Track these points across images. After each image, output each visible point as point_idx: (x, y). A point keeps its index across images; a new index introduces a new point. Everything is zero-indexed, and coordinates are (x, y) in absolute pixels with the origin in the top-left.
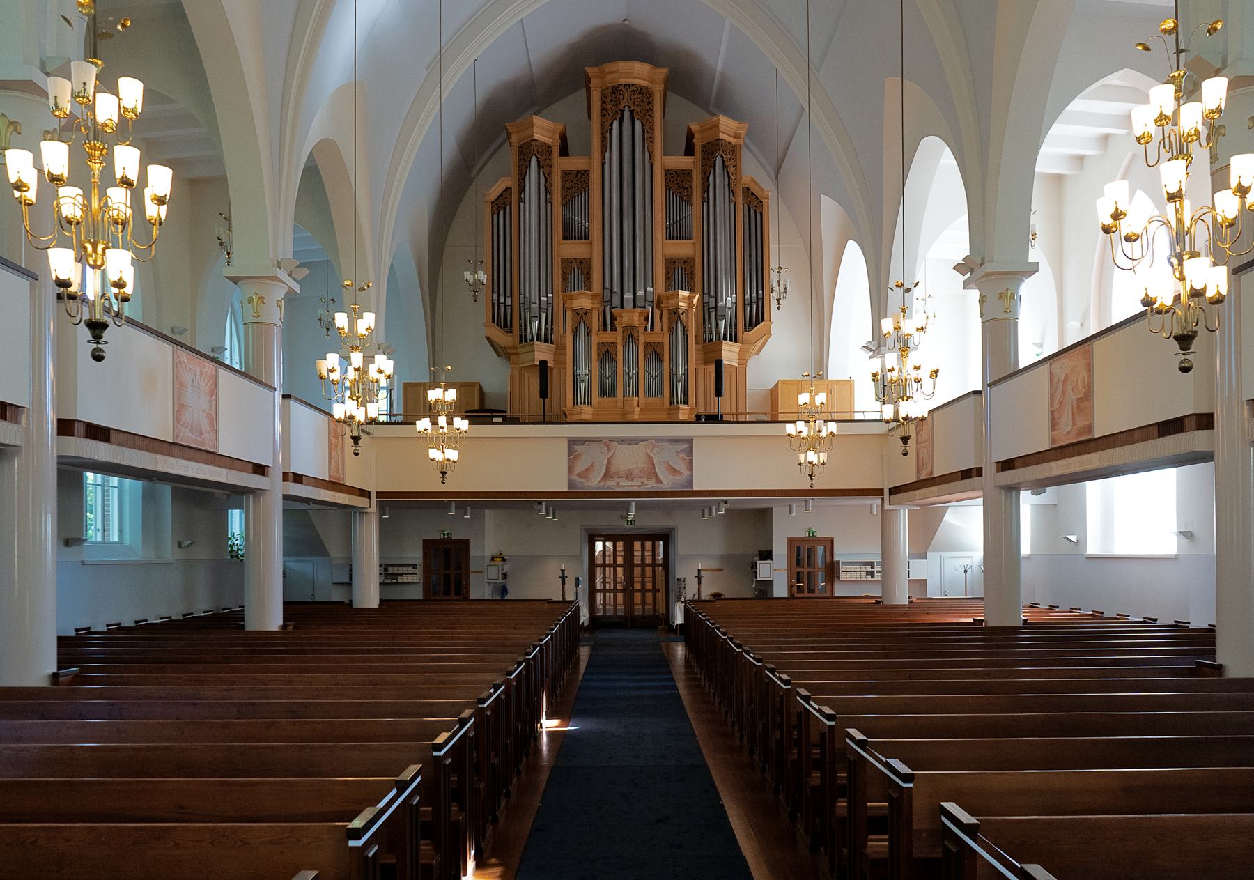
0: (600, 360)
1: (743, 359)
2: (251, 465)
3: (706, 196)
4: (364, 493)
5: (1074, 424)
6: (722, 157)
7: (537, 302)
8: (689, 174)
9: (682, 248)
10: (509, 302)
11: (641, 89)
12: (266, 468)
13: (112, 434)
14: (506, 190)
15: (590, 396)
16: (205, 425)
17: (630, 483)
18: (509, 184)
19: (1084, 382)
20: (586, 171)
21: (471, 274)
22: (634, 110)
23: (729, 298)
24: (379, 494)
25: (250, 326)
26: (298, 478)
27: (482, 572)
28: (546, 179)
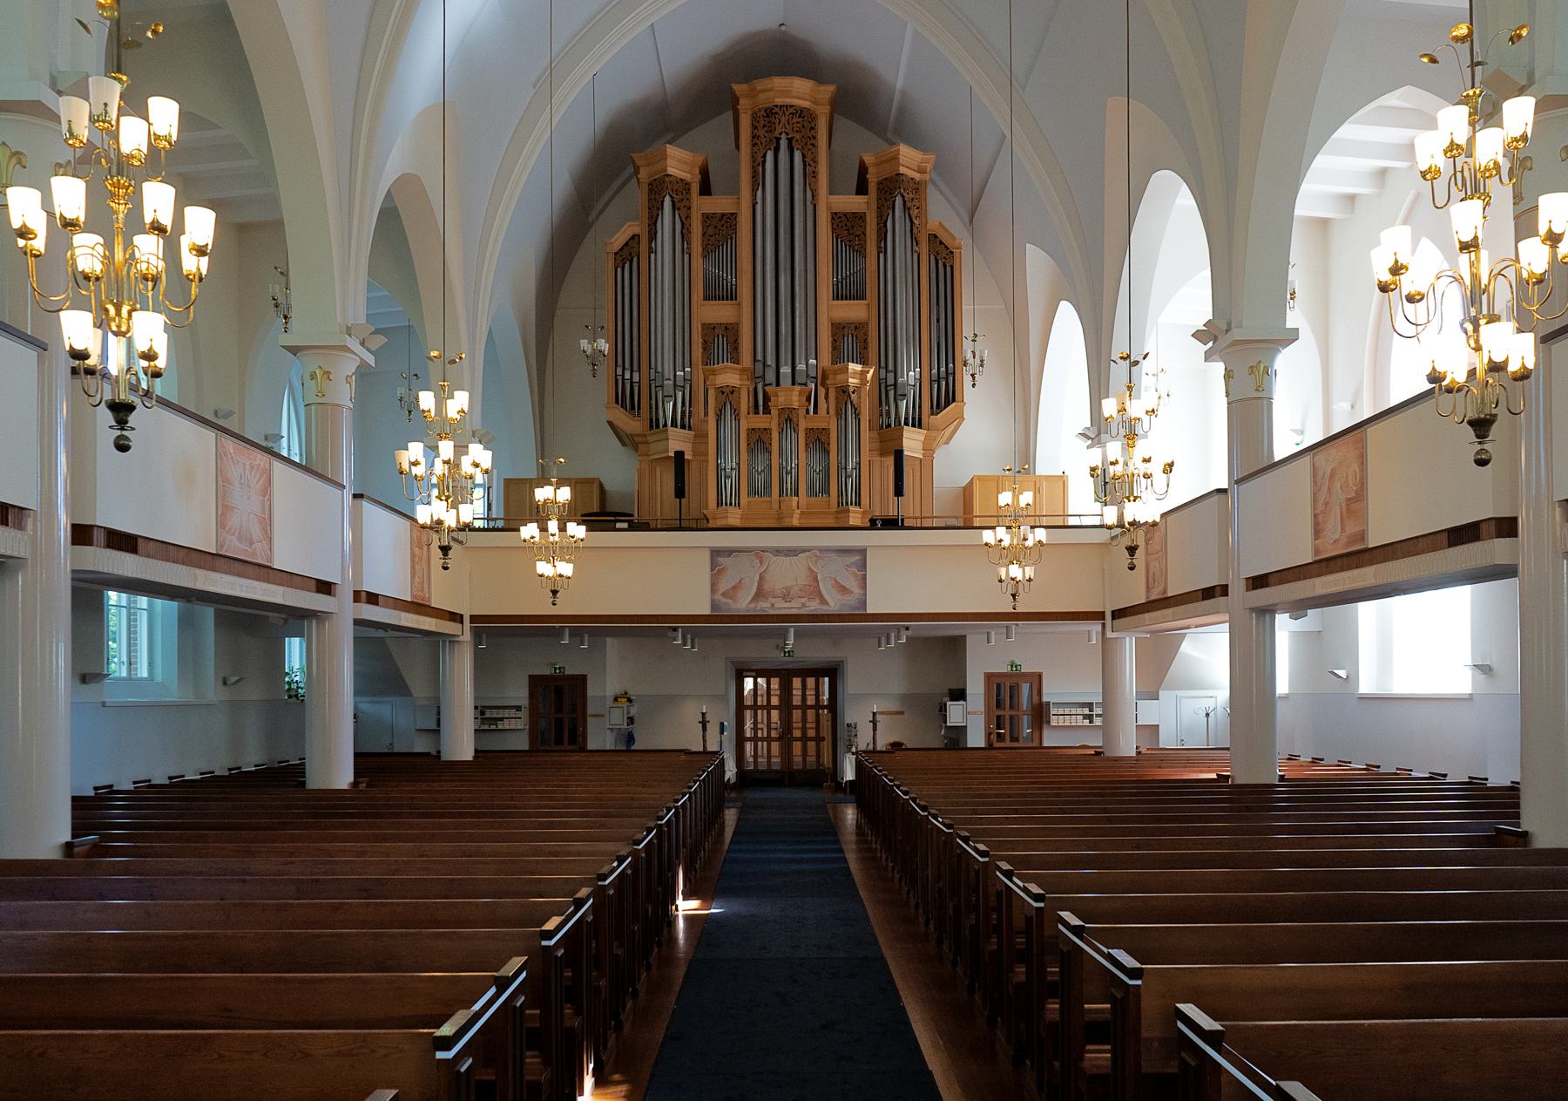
0: (750, 451)
1: (929, 450)
2: (314, 582)
3: (882, 245)
4: (456, 617)
5: (1343, 530)
6: (903, 197)
7: (672, 378)
8: (861, 217)
9: (853, 311)
10: (636, 378)
11: (802, 111)
12: (333, 585)
13: (141, 543)
14: (633, 237)
15: (738, 495)
16: (256, 532)
17: (787, 605)
18: (636, 230)
19: (1356, 478)
20: (732, 214)
21: (589, 343)
22: (792, 138)
23: (912, 373)
24: (474, 618)
25: (313, 407)
26: (373, 599)
27: (603, 716)
28: (683, 224)
